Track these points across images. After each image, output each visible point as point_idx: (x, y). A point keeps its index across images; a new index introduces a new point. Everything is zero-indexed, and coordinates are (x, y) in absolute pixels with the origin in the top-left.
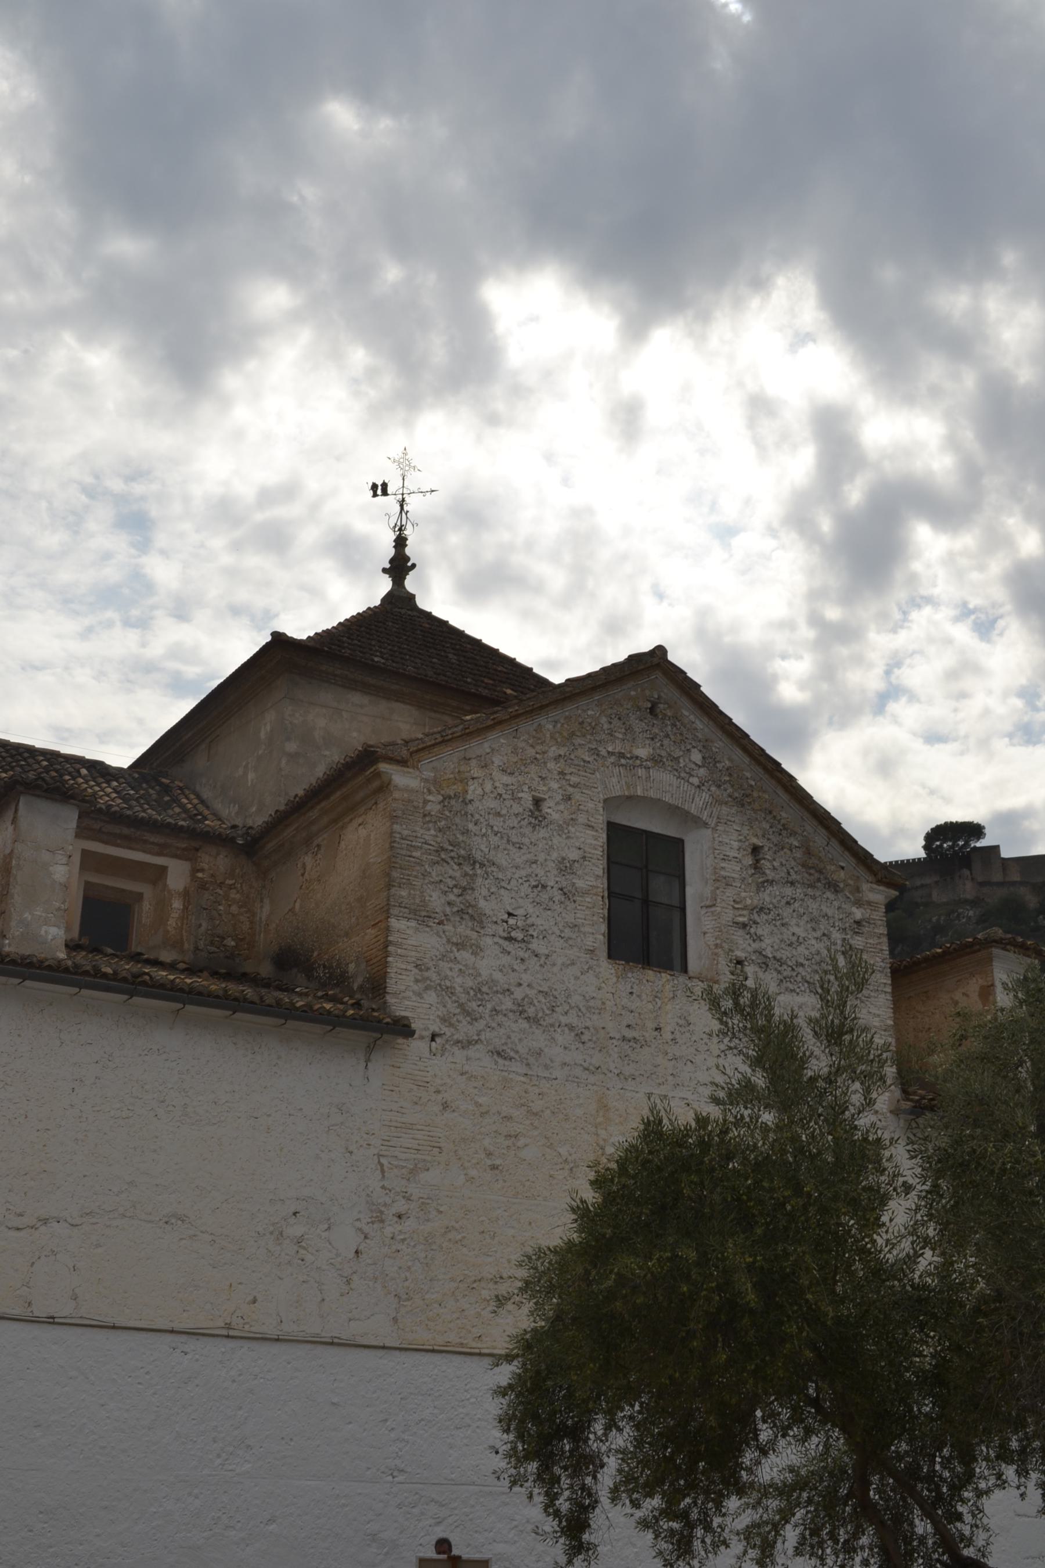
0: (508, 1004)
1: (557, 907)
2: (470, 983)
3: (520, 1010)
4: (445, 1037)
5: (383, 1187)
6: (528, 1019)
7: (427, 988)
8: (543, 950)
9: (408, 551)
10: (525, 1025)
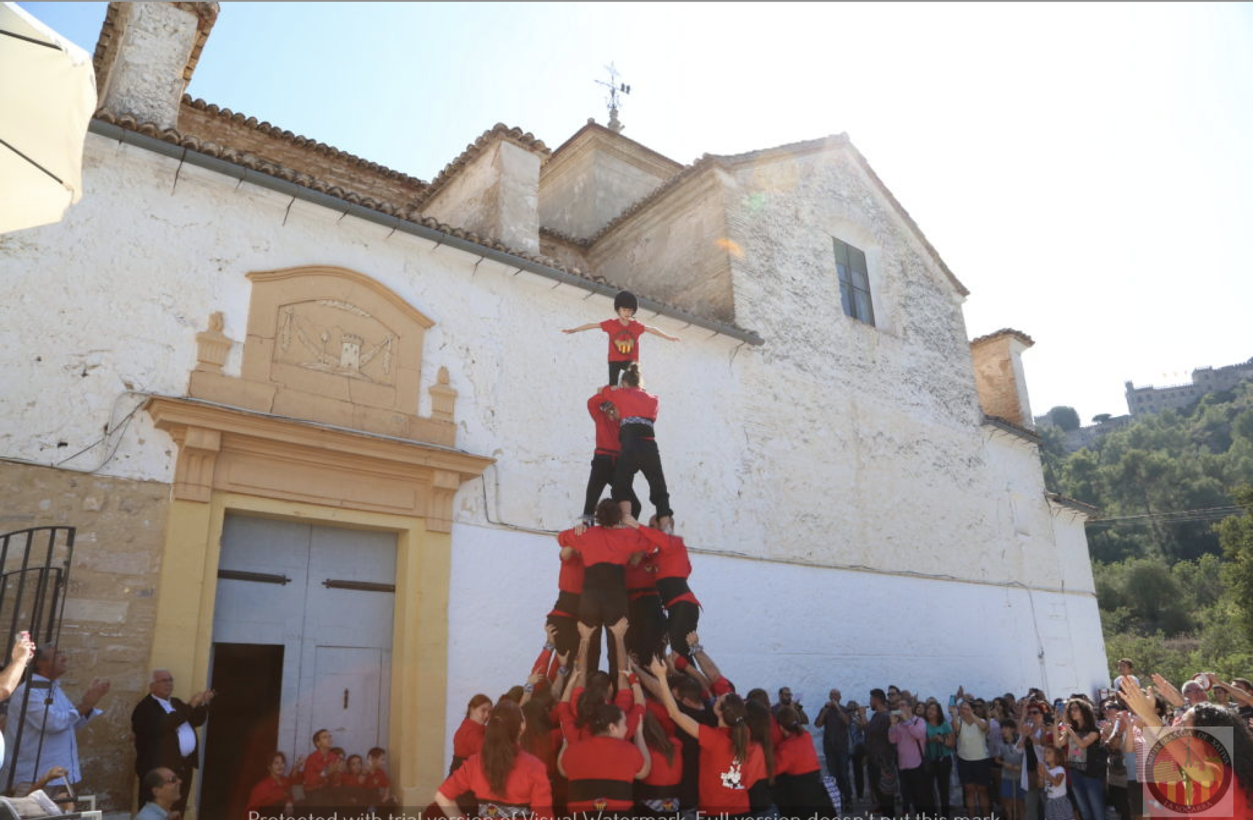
0: (799, 336)
1: (816, 278)
2: (779, 318)
3: (806, 340)
4: (769, 352)
5: (749, 449)
6: (811, 346)
7: (758, 318)
8: (814, 304)
9: (619, 118)
10: (810, 349)
